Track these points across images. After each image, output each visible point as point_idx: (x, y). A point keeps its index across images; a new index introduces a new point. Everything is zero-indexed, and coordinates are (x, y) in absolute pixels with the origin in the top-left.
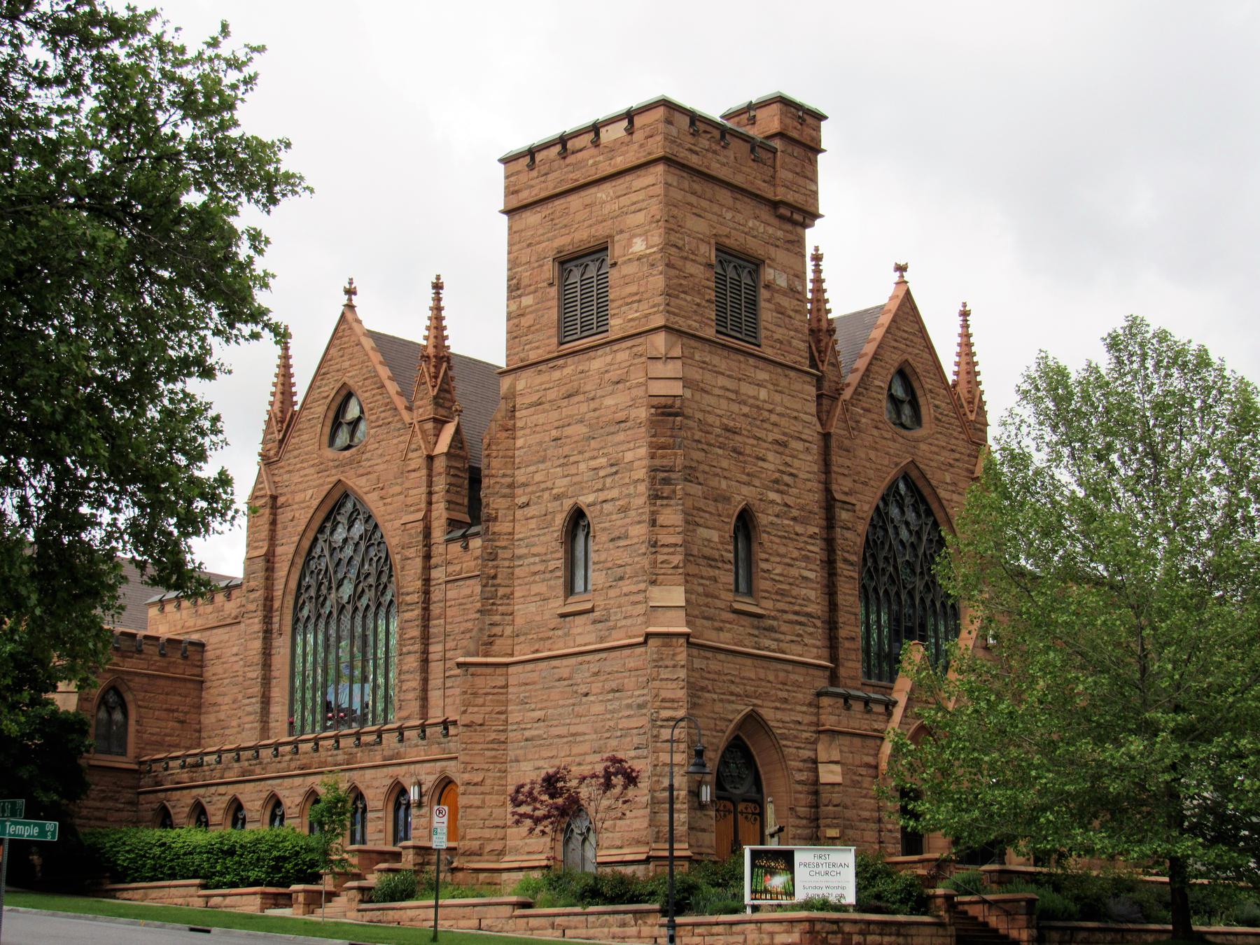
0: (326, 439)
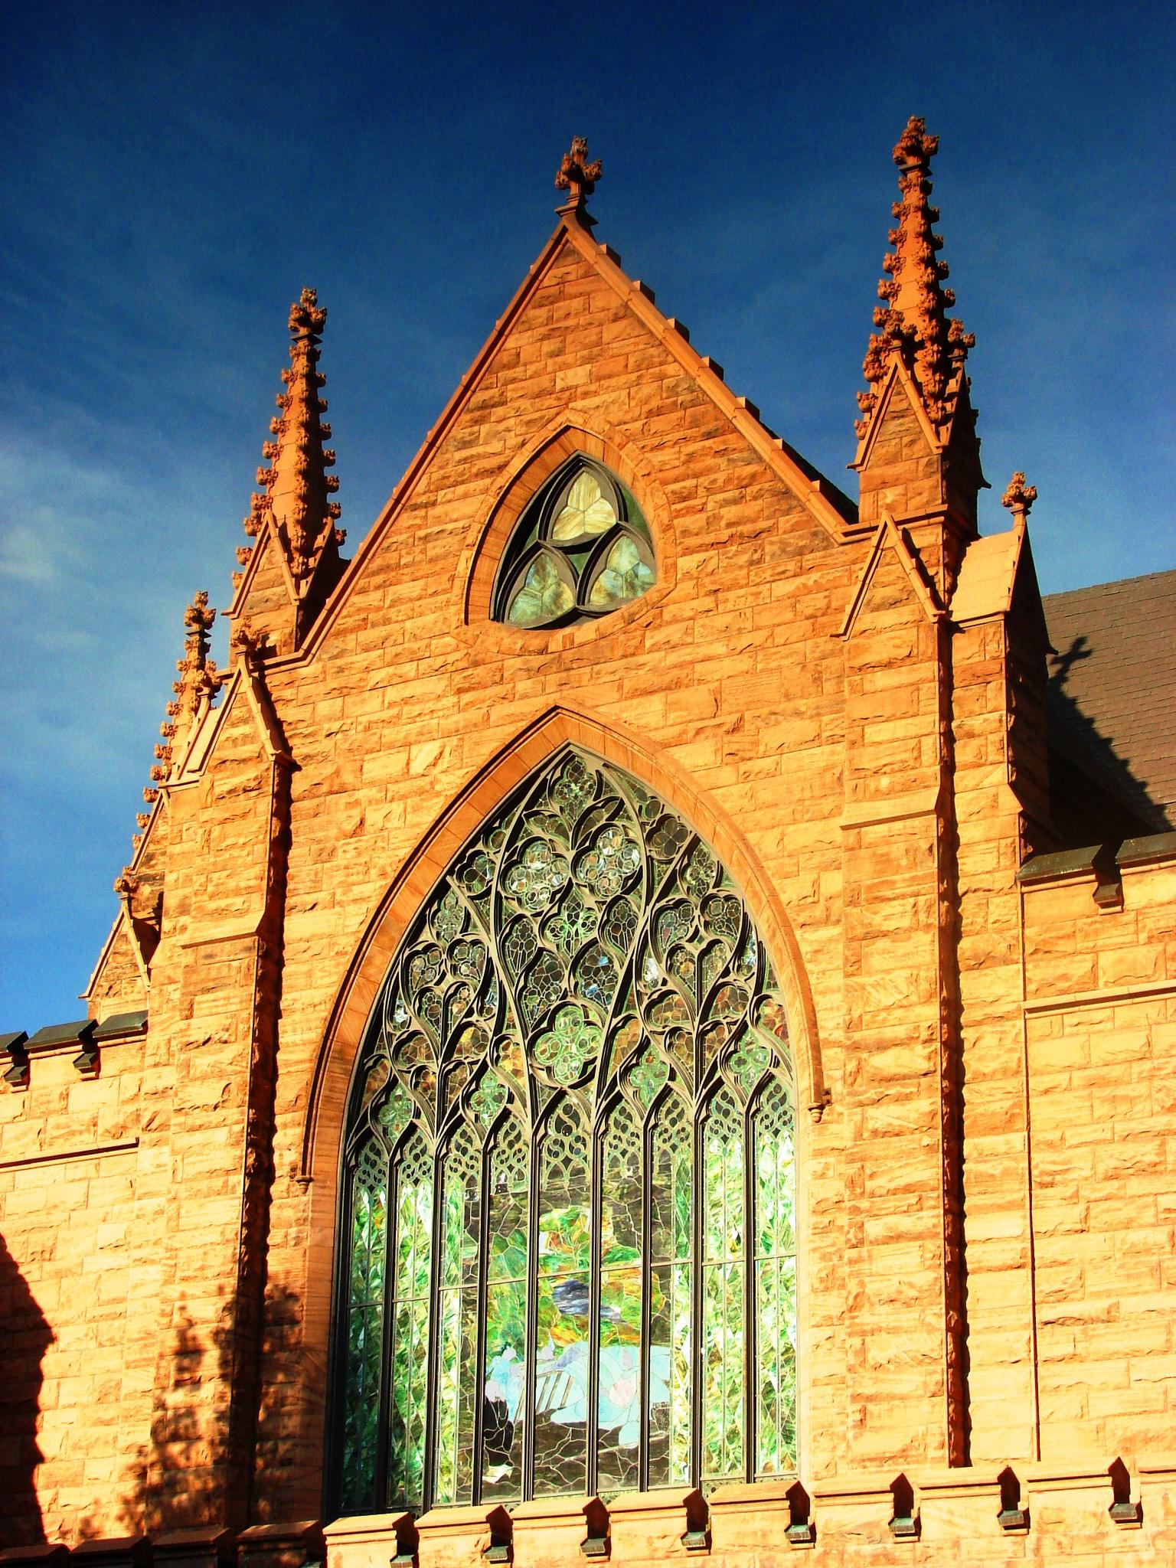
0: (483, 596)
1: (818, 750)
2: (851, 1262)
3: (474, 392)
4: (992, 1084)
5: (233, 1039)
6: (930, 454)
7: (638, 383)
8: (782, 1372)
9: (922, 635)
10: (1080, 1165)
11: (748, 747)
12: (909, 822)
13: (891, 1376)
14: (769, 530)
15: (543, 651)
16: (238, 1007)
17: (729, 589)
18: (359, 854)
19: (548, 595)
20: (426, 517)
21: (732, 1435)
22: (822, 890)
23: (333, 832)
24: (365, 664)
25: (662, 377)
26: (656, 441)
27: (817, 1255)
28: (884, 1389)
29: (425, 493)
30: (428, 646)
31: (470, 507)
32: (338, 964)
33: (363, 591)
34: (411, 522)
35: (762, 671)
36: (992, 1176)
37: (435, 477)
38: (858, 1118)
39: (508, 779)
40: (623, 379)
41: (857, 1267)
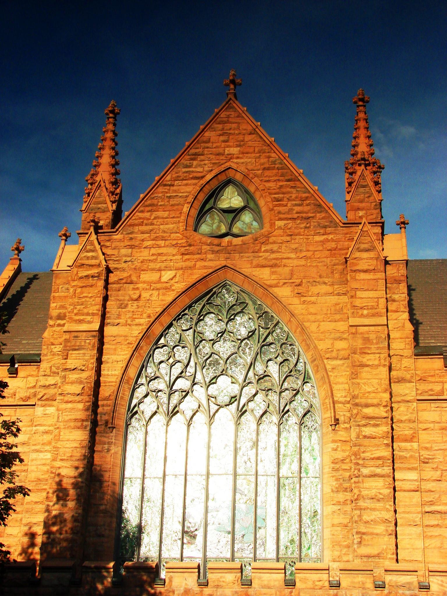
1: (333, 297)
2: (355, 482)
3: (191, 149)
4: (405, 424)
5: (86, 369)
6: (376, 202)
7: (259, 157)
8: (313, 520)
9: (379, 263)
10: (438, 457)
11: (305, 292)
12: (376, 327)
13: (372, 526)
14: (313, 217)
15: (219, 245)
16: (89, 358)
17: (296, 235)
18: (138, 308)
19: (215, 226)
20: (169, 190)
21: (292, 541)
22: (335, 347)
23: (127, 298)
24: (142, 238)
25: (269, 157)
26: (267, 179)
27: (334, 478)
28: (370, 530)
29: (169, 181)
30: (170, 236)
31: (189, 189)
32: (129, 347)
33: (142, 212)
34: (163, 190)
35: (310, 266)
36: (406, 457)
37: (174, 176)
38: (357, 430)
39: (202, 289)
40: (253, 155)
41: (357, 485)
